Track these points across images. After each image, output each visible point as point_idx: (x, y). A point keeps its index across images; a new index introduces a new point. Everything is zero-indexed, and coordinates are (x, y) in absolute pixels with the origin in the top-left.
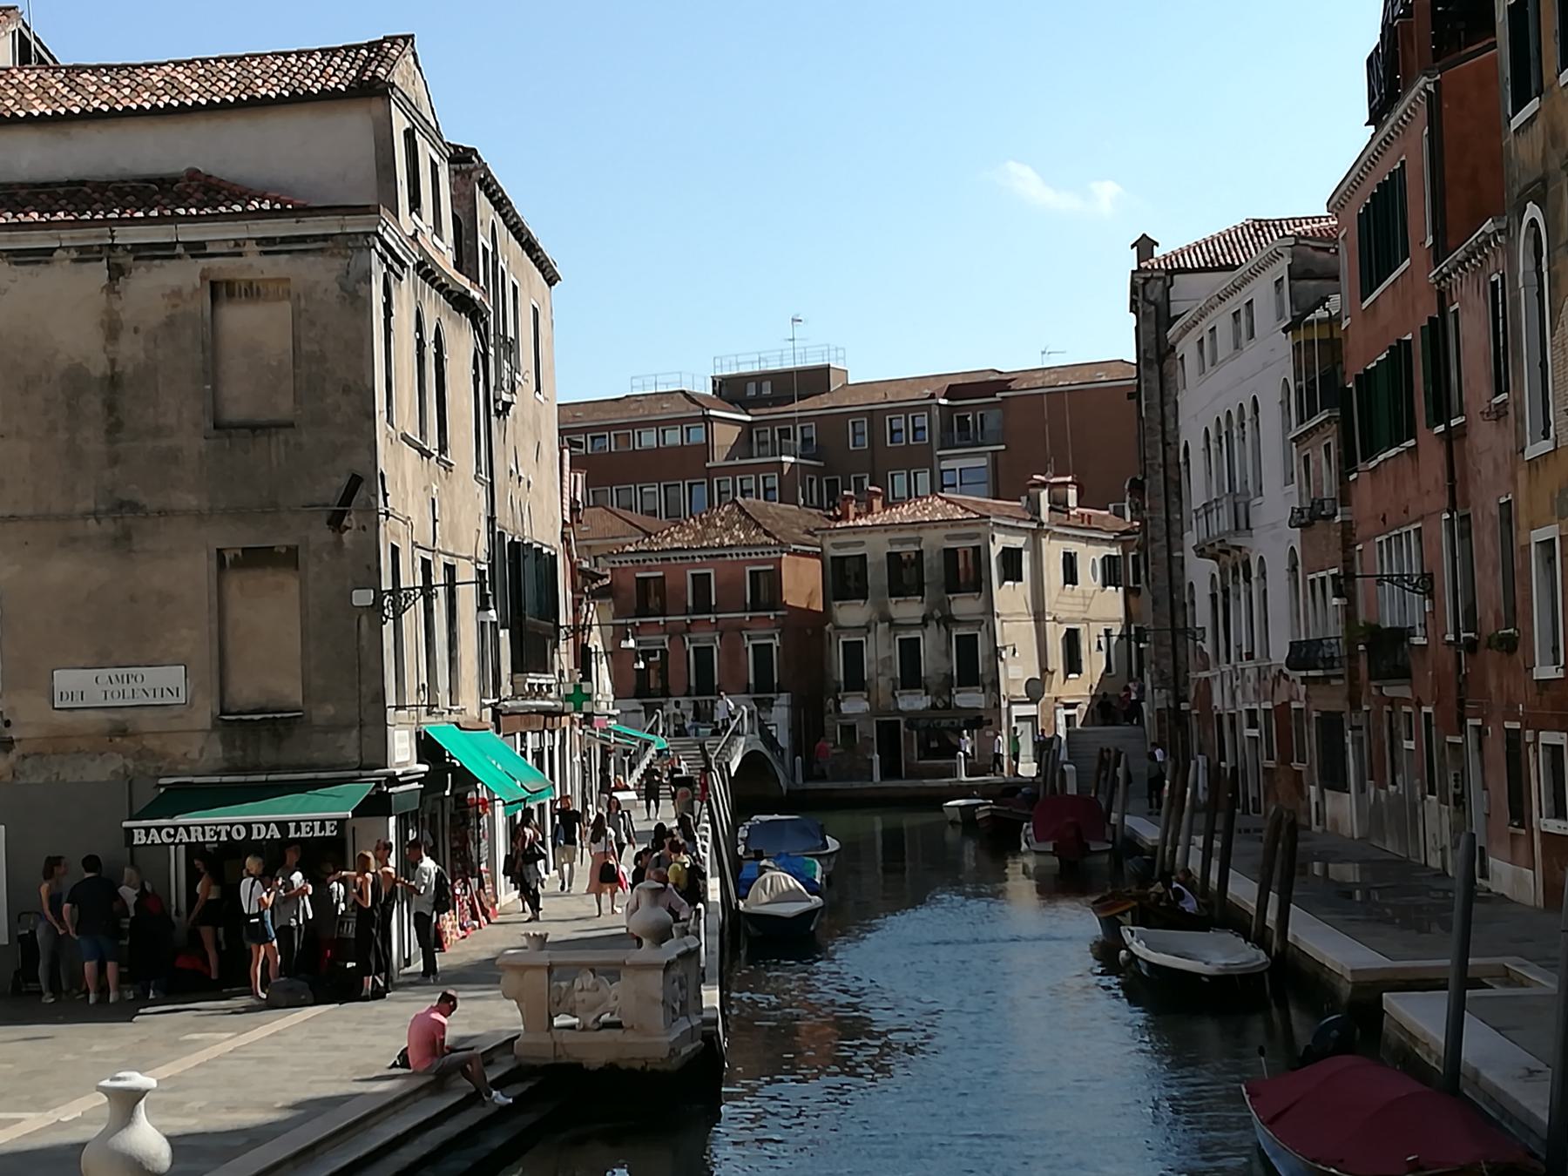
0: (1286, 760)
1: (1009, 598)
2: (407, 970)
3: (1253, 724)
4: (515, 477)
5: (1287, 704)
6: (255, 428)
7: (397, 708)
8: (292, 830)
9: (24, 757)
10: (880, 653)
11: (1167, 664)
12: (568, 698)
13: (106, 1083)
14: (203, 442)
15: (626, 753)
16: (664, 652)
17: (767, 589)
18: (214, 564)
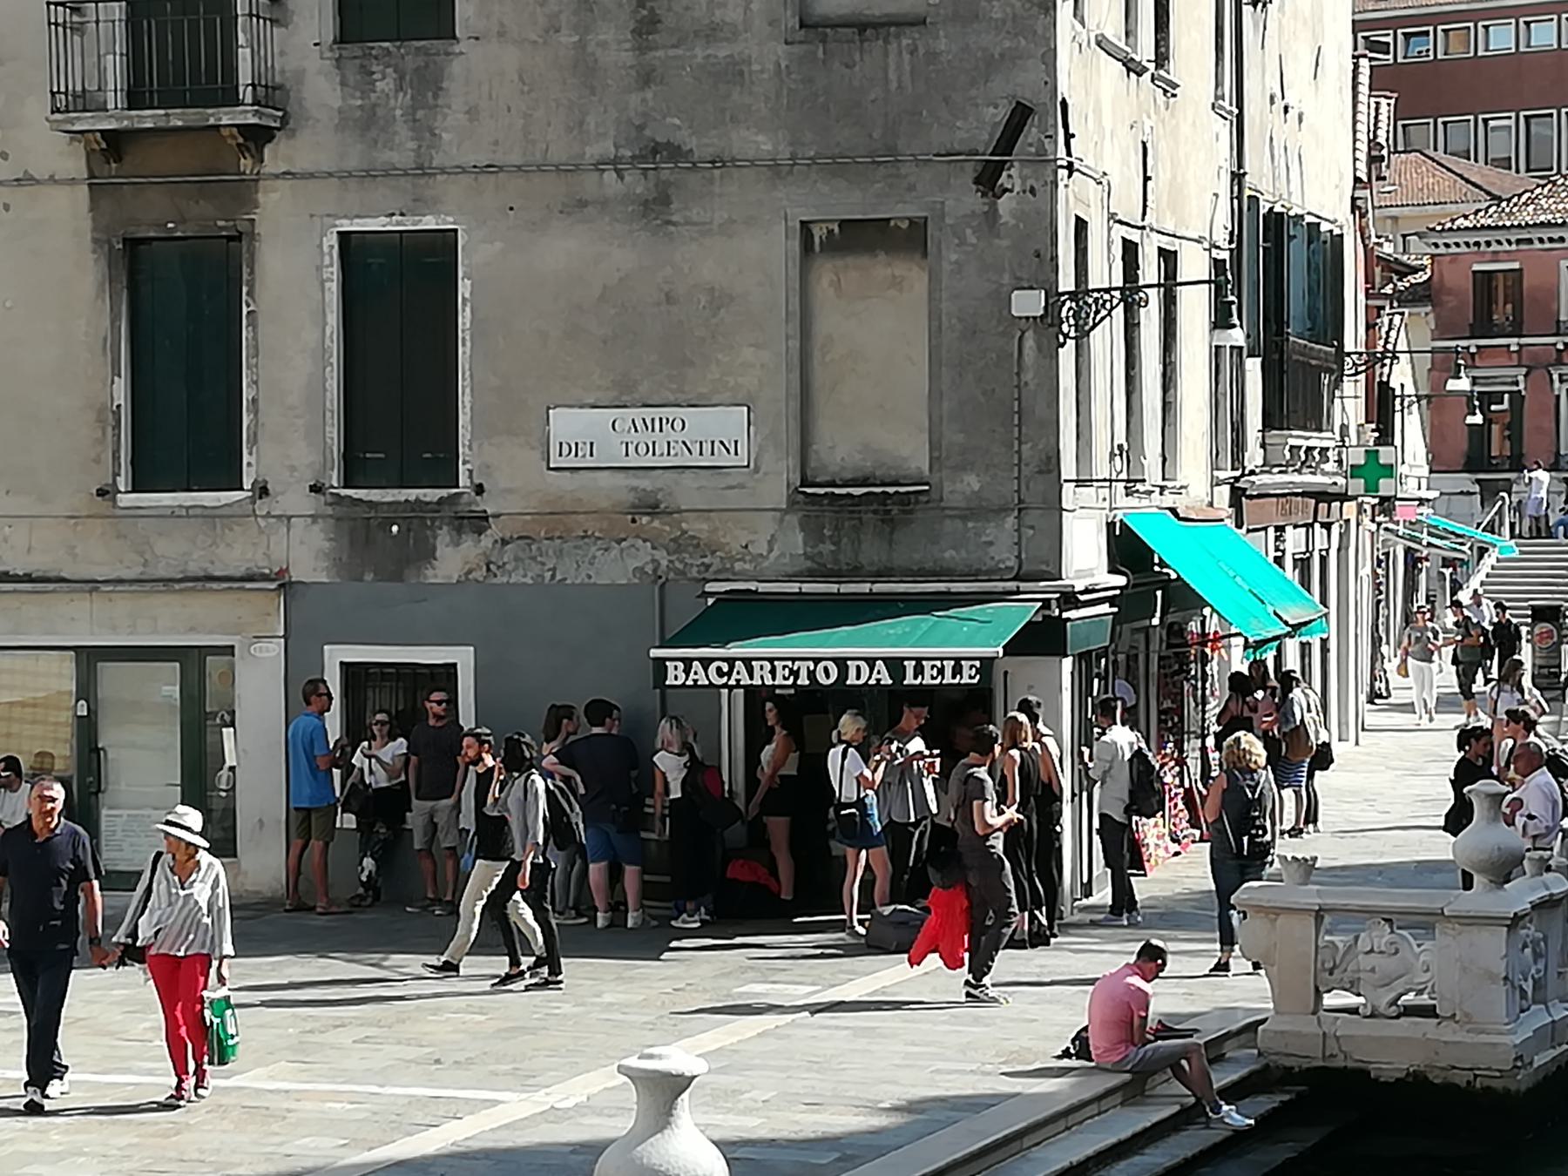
2: (1085, 902)
4: (1280, 105)
7: (1079, 483)
8: (910, 672)
9: (504, 542)
12: (1356, 471)
13: (633, 1062)
14: (781, 49)
15: (1447, 562)
16: (1517, 398)
18: (796, 244)
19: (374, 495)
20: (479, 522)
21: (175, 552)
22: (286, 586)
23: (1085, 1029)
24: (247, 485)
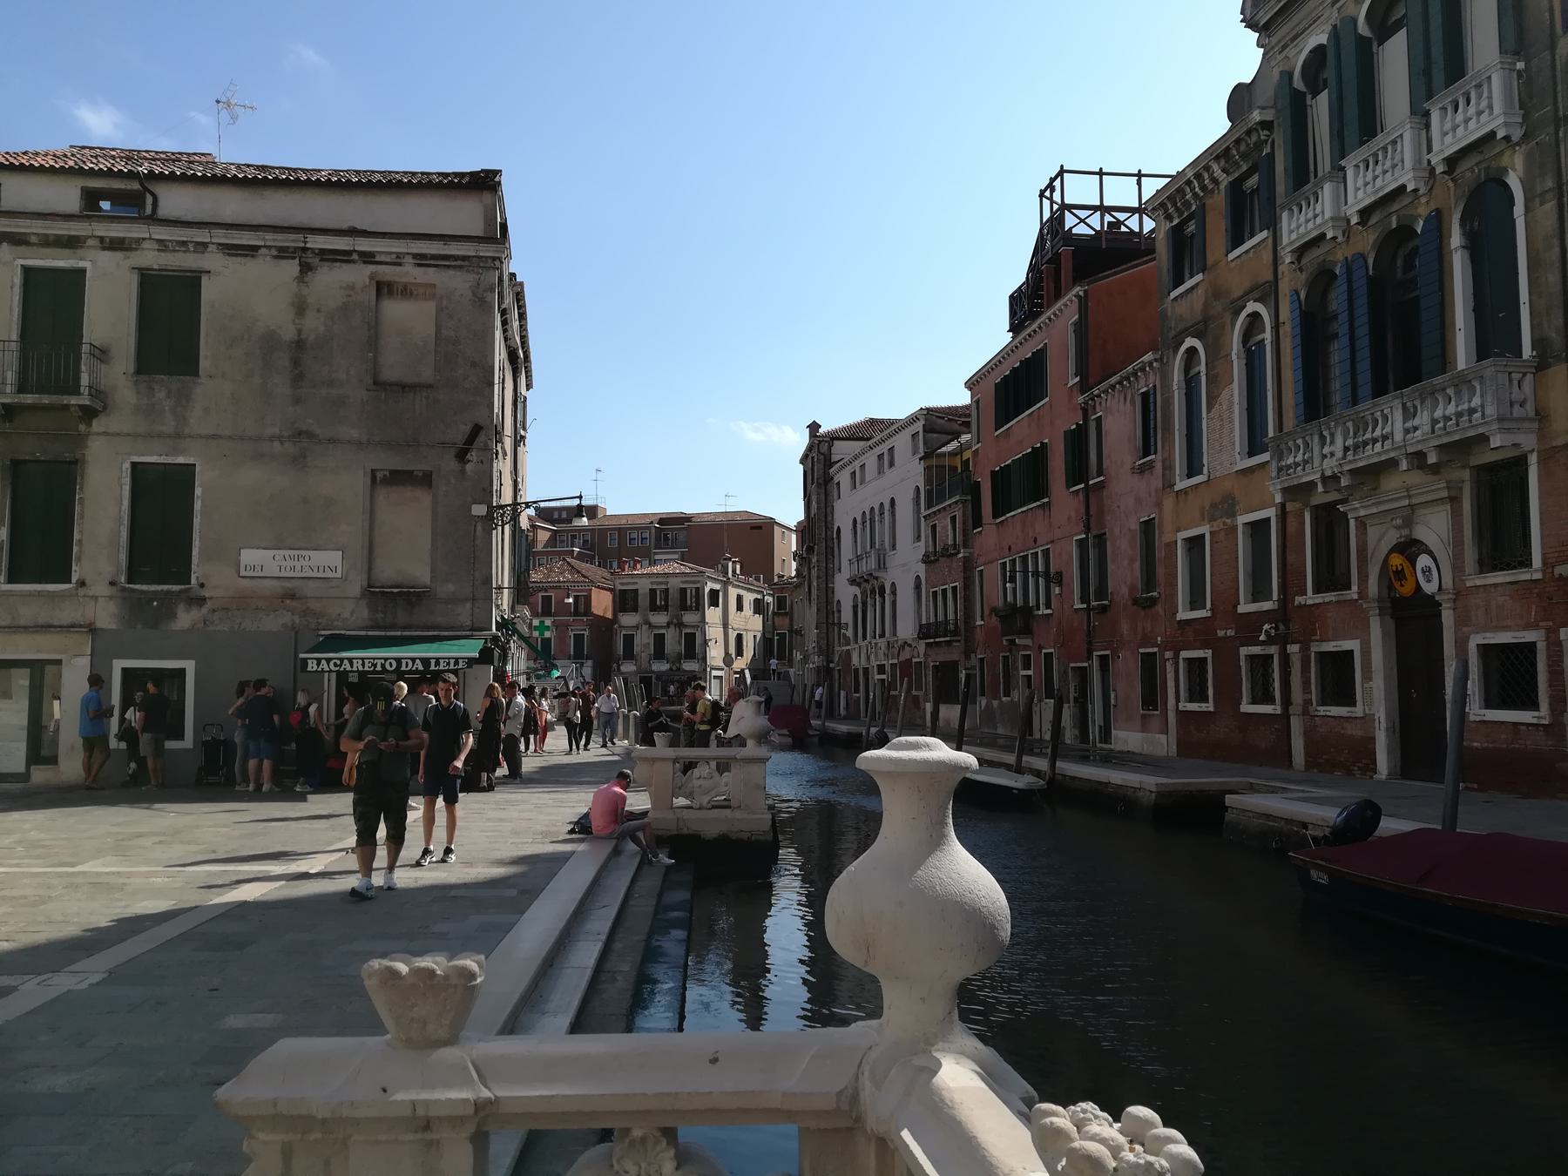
1: (713, 615)
5: (909, 661)
6: (404, 387)
10: (643, 640)
17: (584, 603)
19: (145, 587)
20: (201, 601)
21: (27, 614)
22: (92, 630)
23: (586, 815)
24: (74, 580)
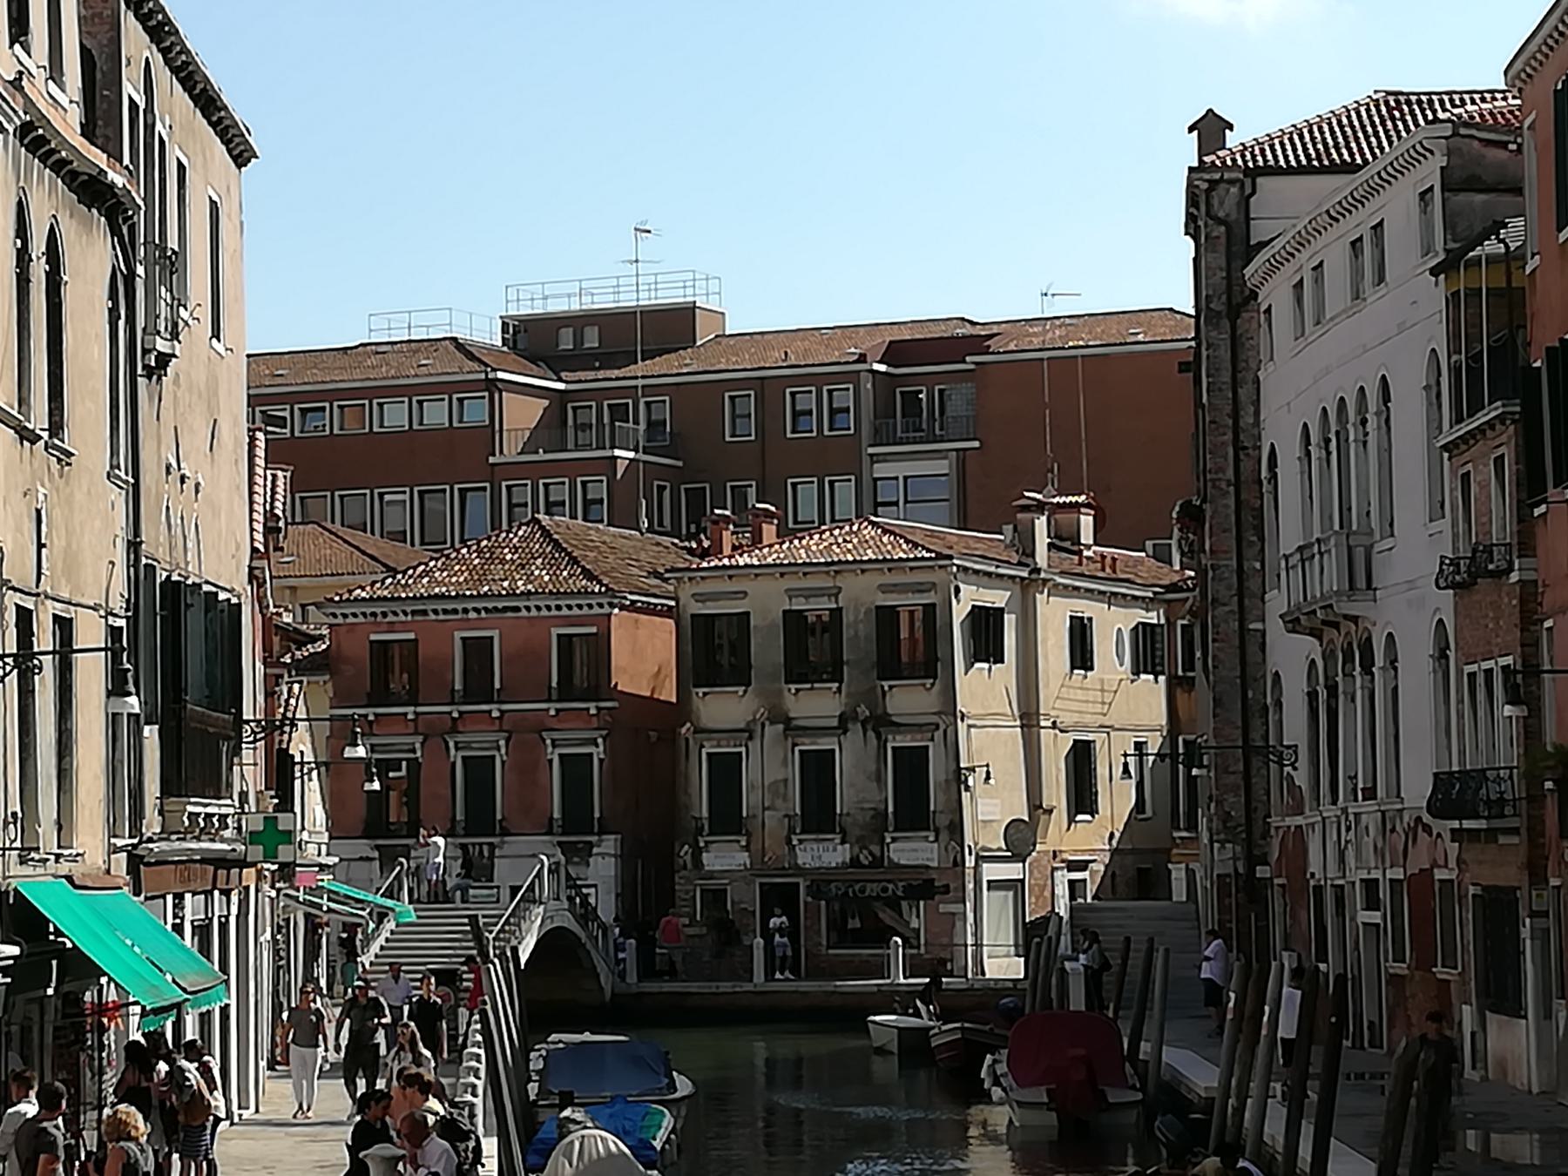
0: (1424, 962)
1: (982, 690)
3: (1372, 903)
5: (1427, 874)
10: (769, 772)
11: (1235, 804)
17: (585, 664)
